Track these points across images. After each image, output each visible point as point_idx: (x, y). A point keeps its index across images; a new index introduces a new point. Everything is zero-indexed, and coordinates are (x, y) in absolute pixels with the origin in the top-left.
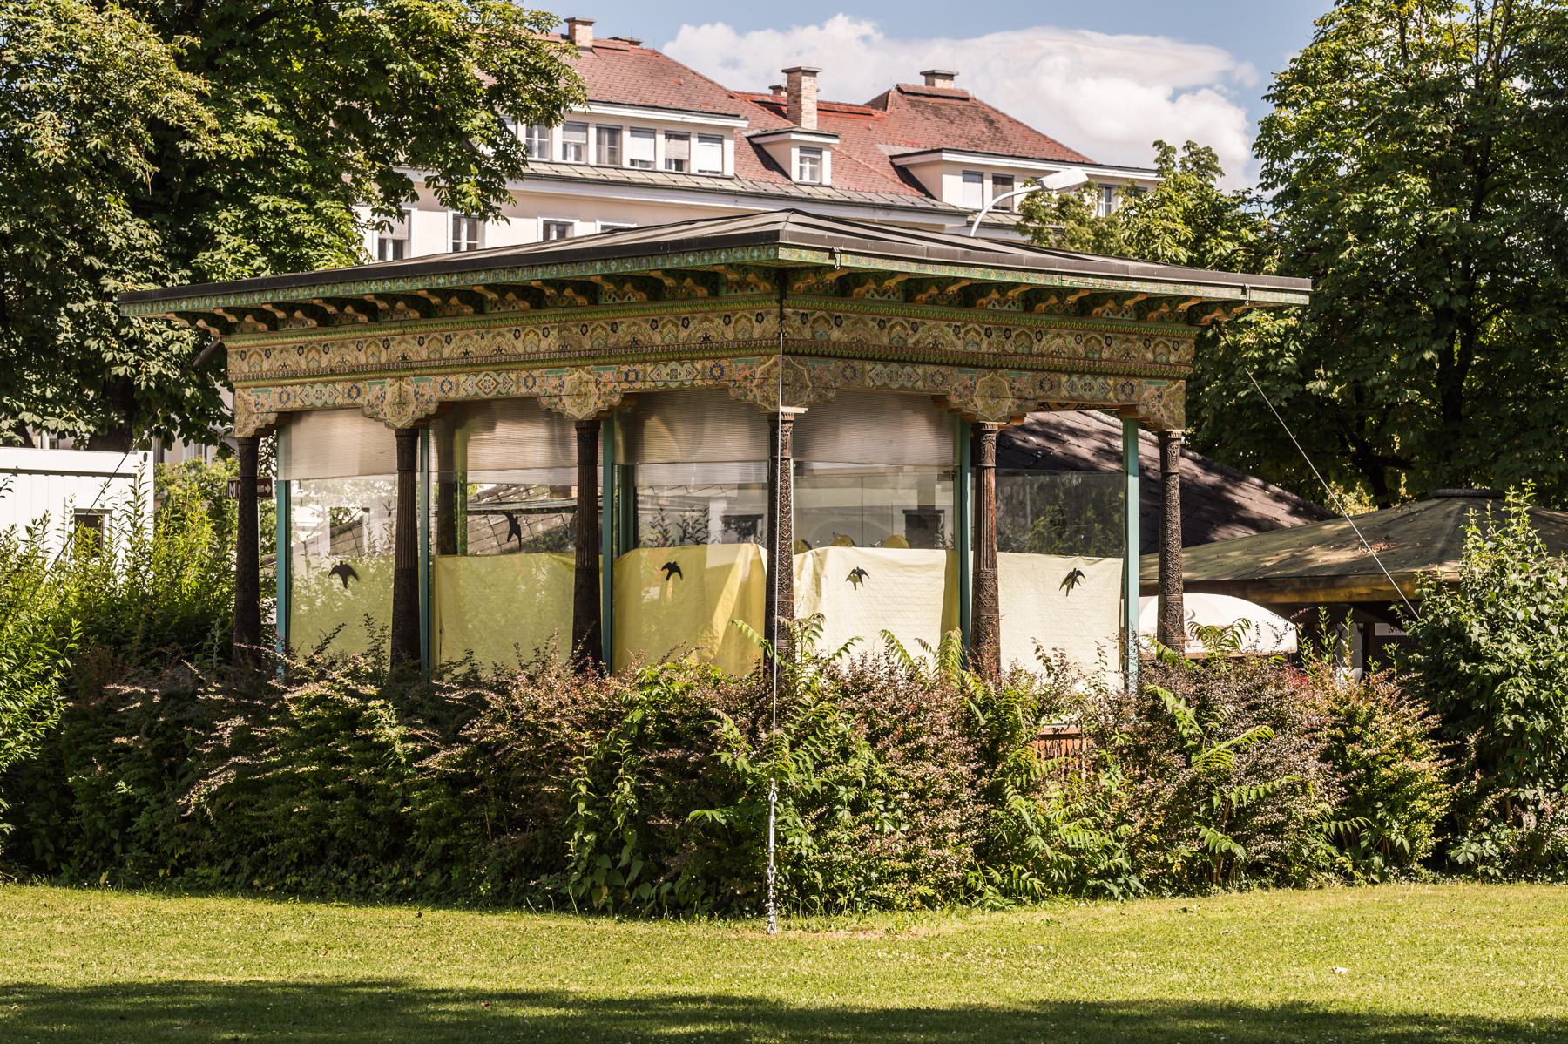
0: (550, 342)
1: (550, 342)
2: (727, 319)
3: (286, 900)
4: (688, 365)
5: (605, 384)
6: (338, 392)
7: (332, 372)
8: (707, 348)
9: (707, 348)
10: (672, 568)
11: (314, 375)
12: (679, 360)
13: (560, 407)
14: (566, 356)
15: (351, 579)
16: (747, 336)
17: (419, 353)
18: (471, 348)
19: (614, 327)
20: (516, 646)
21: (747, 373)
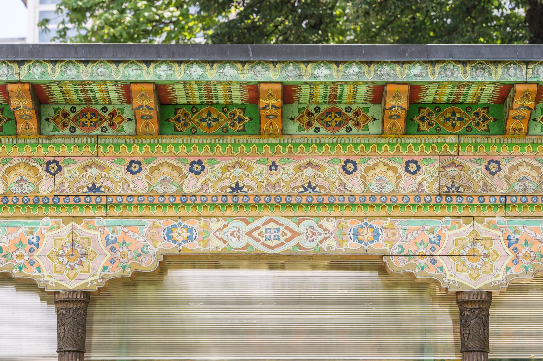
0: (429, 178)
13: (432, 272)
14: (451, 197)
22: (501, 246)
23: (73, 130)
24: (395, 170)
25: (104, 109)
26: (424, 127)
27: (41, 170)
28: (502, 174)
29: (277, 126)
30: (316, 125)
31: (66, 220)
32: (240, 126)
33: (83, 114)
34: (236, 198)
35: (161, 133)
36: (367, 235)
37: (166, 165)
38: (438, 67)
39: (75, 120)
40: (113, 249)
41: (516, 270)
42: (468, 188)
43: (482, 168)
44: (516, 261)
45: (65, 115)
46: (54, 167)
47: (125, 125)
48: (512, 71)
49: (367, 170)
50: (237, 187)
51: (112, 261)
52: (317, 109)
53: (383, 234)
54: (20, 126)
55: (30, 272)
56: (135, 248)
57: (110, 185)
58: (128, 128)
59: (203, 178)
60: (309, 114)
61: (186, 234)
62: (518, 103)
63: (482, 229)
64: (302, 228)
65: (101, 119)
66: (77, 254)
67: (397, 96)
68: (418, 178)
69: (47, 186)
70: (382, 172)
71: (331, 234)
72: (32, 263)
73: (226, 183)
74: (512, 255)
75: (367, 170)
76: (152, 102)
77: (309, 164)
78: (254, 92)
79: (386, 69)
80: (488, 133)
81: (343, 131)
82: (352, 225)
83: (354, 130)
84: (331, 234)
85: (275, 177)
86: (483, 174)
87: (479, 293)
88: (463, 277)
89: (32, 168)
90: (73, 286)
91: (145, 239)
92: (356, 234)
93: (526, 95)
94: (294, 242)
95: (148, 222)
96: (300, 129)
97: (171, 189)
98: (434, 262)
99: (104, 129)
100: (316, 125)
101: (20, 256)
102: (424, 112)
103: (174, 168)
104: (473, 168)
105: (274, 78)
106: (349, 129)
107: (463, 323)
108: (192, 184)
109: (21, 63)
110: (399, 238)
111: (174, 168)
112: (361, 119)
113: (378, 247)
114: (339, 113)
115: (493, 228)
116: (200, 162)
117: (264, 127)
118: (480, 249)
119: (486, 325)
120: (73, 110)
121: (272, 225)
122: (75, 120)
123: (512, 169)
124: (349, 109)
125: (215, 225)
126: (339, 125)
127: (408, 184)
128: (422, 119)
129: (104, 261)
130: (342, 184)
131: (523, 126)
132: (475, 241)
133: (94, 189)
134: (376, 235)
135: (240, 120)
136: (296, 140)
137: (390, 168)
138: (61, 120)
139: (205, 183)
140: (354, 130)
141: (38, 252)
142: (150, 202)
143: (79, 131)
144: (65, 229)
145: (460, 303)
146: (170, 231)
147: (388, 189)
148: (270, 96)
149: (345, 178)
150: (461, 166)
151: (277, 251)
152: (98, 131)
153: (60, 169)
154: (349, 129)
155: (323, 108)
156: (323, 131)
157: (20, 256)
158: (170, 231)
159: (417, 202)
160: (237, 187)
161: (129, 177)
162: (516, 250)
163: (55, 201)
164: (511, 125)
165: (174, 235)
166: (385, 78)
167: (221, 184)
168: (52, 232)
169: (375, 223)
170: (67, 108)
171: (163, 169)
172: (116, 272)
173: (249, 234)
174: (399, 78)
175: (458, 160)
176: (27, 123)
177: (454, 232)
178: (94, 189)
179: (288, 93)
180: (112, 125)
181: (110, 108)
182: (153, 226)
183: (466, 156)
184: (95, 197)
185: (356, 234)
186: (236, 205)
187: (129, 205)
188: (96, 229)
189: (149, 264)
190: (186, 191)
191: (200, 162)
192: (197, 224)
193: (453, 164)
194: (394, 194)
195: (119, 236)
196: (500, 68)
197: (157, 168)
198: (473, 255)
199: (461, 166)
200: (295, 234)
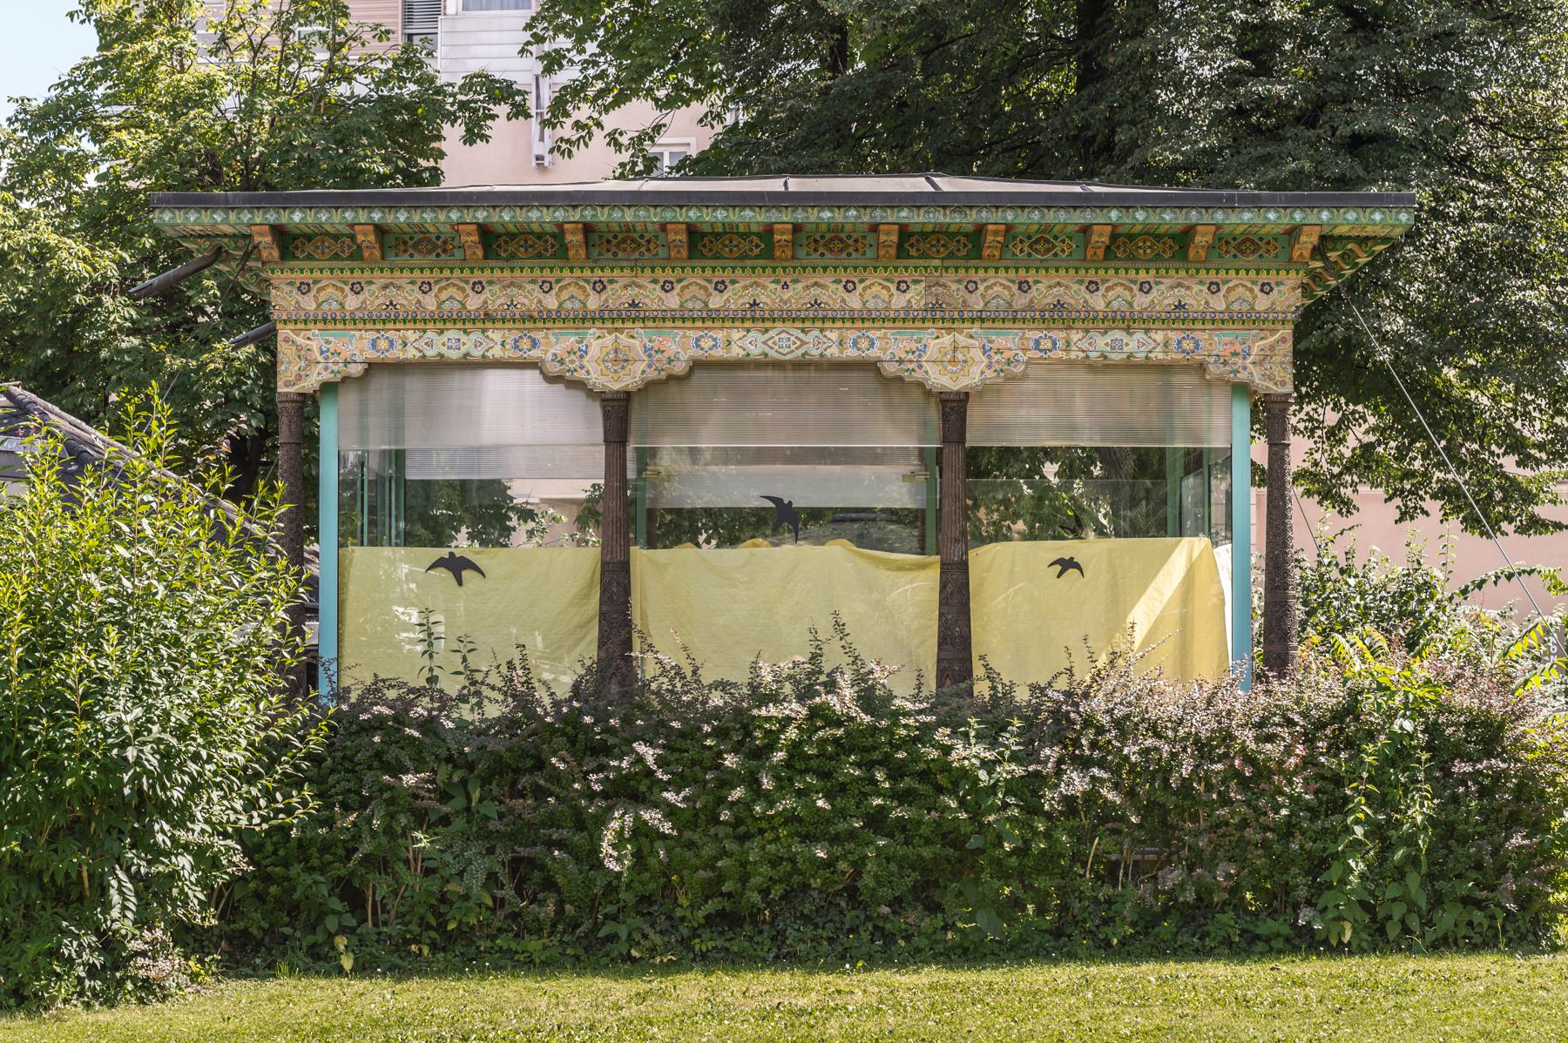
0: (916, 296)
1: (916, 296)
2: (1214, 287)
3: (691, 969)
4: (1139, 335)
5: (999, 351)
6: (496, 343)
7: (488, 317)
8: (1179, 316)
9: (1179, 316)
10: (1067, 564)
11: (464, 320)
12: (1128, 330)
13: (918, 375)
14: (938, 315)
15: (466, 574)
16: (1245, 307)
17: (408, 297)
18: (763, 299)
19: (1024, 286)
20: (685, 649)
21: (1238, 348)
22: (977, 354)
23: (615, 254)
24: (888, 289)
25: (642, 237)
26: (913, 252)
27: (589, 288)
28: (978, 292)
29: (789, 253)
30: (821, 250)
31: (610, 331)
32: (757, 251)
33: (624, 241)
34: (753, 316)
35: (690, 257)
36: (864, 344)
37: (693, 288)
38: (922, 212)
39: (617, 246)
40: (650, 356)
41: (989, 374)
42: (948, 304)
43: (962, 287)
44: (989, 366)
45: (608, 242)
46: (600, 286)
47: (660, 250)
48: (984, 214)
49: (865, 289)
50: (755, 304)
51: (649, 366)
52: (823, 237)
53: (877, 343)
54: (571, 253)
55: (581, 375)
56: (670, 353)
57: (648, 301)
58: (662, 253)
59: (726, 295)
60: (816, 241)
61: (711, 343)
62: (990, 238)
63: (962, 339)
64: (809, 338)
65: (639, 245)
66: (620, 359)
67: (888, 233)
68: (908, 296)
69: (594, 302)
70: (876, 292)
71: (471, 767)
72: (582, 367)
73: (746, 300)
74: (986, 361)
75: (865, 289)
76: (684, 237)
77: (816, 284)
78: (769, 230)
79: (878, 212)
80: (967, 257)
81: (844, 255)
82: (851, 335)
83: (854, 255)
84: (471, 767)
85: (786, 295)
86: (963, 292)
87: (958, 393)
88: (942, 379)
89: (581, 287)
90: (616, 387)
91: (680, 346)
92: (855, 343)
93: (996, 233)
94: (802, 351)
95: (681, 332)
96: (808, 254)
97: (699, 305)
98: (920, 367)
99: (642, 254)
100: (821, 250)
101: (572, 362)
102: (913, 240)
103: (701, 287)
104: (954, 287)
105: (785, 219)
106: (849, 254)
107: (945, 418)
108: (716, 301)
109: (575, 207)
110: (887, 346)
111: (701, 287)
112: (859, 245)
113: (875, 353)
114: (841, 240)
115: (969, 340)
116: (723, 282)
117: (778, 254)
118: (960, 356)
119: (964, 420)
120: (615, 237)
121: (783, 335)
122: (617, 246)
123: (987, 288)
124: (849, 237)
125: (736, 335)
126: (841, 251)
127: (899, 301)
128: (912, 246)
129: (642, 366)
130: (843, 301)
131: (997, 254)
132: (955, 349)
133: (633, 305)
134: (872, 344)
135: (757, 246)
136: (804, 263)
137: (884, 287)
138: (605, 246)
139: (728, 300)
140: (854, 255)
141: (587, 358)
142: (681, 318)
143: (620, 255)
144: (609, 339)
145: (943, 402)
146: (698, 340)
147: (881, 305)
148: (783, 233)
149: (846, 295)
150: (944, 286)
151: (789, 357)
152: (636, 255)
153: (605, 287)
154: (849, 254)
155: (828, 236)
156: (828, 255)
157: (572, 362)
158: (698, 340)
159: (906, 319)
160: (755, 304)
161: (663, 295)
162: (989, 357)
163: (600, 317)
164: (986, 252)
165: (702, 344)
166: (878, 220)
167: (741, 301)
168: (598, 343)
169: (871, 334)
170: (610, 236)
171: (693, 288)
172: (652, 375)
173: (765, 343)
174: (890, 220)
175: (942, 281)
176: (577, 251)
177: (936, 343)
178: (633, 305)
179: (797, 228)
180: (648, 250)
181: (647, 237)
182: (684, 336)
183: (948, 278)
184: (634, 314)
185: (855, 343)
186: (754, 320)
187: (664, 319)
188: (636, 340)
189: (680, 368)
190: (711, 306)
191: (723, 282)
192: (720, 335)
193: (937, 284)
194: (887, 309)
195: (656, 345)
196: (974, 211)
197: (687, 287)
198: (954, 361)
199: (944, 286)
200: (804, 343)
